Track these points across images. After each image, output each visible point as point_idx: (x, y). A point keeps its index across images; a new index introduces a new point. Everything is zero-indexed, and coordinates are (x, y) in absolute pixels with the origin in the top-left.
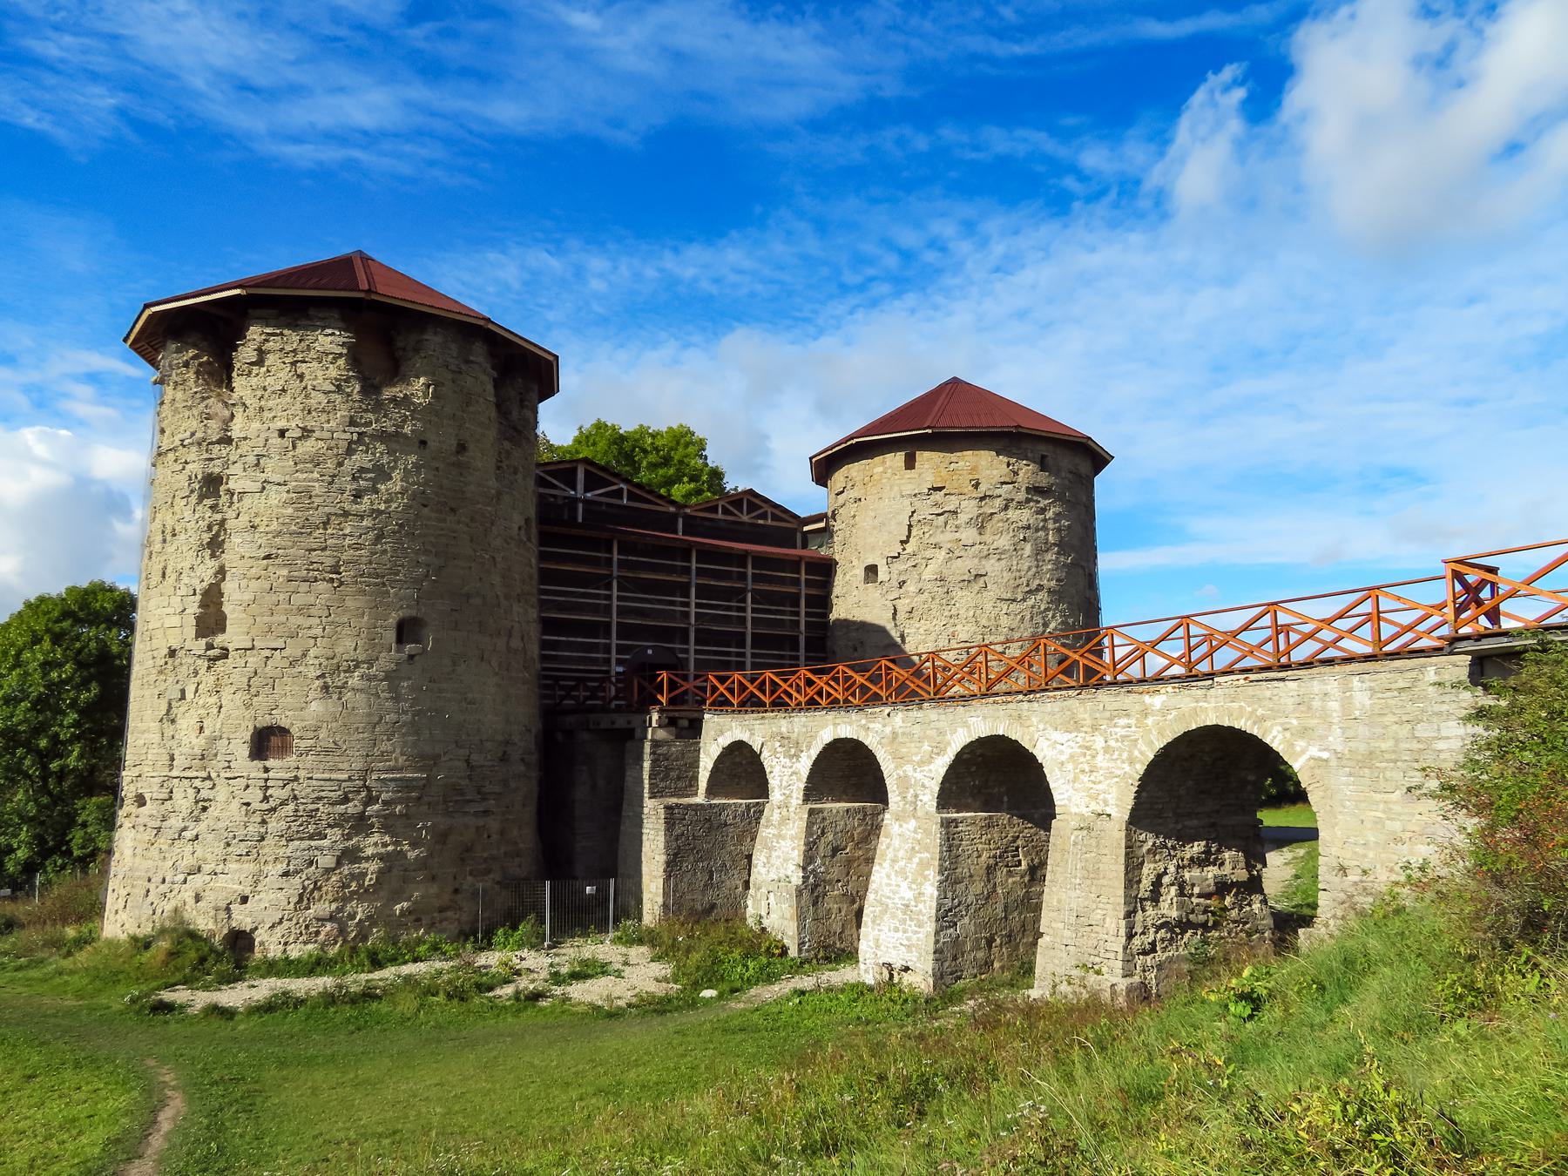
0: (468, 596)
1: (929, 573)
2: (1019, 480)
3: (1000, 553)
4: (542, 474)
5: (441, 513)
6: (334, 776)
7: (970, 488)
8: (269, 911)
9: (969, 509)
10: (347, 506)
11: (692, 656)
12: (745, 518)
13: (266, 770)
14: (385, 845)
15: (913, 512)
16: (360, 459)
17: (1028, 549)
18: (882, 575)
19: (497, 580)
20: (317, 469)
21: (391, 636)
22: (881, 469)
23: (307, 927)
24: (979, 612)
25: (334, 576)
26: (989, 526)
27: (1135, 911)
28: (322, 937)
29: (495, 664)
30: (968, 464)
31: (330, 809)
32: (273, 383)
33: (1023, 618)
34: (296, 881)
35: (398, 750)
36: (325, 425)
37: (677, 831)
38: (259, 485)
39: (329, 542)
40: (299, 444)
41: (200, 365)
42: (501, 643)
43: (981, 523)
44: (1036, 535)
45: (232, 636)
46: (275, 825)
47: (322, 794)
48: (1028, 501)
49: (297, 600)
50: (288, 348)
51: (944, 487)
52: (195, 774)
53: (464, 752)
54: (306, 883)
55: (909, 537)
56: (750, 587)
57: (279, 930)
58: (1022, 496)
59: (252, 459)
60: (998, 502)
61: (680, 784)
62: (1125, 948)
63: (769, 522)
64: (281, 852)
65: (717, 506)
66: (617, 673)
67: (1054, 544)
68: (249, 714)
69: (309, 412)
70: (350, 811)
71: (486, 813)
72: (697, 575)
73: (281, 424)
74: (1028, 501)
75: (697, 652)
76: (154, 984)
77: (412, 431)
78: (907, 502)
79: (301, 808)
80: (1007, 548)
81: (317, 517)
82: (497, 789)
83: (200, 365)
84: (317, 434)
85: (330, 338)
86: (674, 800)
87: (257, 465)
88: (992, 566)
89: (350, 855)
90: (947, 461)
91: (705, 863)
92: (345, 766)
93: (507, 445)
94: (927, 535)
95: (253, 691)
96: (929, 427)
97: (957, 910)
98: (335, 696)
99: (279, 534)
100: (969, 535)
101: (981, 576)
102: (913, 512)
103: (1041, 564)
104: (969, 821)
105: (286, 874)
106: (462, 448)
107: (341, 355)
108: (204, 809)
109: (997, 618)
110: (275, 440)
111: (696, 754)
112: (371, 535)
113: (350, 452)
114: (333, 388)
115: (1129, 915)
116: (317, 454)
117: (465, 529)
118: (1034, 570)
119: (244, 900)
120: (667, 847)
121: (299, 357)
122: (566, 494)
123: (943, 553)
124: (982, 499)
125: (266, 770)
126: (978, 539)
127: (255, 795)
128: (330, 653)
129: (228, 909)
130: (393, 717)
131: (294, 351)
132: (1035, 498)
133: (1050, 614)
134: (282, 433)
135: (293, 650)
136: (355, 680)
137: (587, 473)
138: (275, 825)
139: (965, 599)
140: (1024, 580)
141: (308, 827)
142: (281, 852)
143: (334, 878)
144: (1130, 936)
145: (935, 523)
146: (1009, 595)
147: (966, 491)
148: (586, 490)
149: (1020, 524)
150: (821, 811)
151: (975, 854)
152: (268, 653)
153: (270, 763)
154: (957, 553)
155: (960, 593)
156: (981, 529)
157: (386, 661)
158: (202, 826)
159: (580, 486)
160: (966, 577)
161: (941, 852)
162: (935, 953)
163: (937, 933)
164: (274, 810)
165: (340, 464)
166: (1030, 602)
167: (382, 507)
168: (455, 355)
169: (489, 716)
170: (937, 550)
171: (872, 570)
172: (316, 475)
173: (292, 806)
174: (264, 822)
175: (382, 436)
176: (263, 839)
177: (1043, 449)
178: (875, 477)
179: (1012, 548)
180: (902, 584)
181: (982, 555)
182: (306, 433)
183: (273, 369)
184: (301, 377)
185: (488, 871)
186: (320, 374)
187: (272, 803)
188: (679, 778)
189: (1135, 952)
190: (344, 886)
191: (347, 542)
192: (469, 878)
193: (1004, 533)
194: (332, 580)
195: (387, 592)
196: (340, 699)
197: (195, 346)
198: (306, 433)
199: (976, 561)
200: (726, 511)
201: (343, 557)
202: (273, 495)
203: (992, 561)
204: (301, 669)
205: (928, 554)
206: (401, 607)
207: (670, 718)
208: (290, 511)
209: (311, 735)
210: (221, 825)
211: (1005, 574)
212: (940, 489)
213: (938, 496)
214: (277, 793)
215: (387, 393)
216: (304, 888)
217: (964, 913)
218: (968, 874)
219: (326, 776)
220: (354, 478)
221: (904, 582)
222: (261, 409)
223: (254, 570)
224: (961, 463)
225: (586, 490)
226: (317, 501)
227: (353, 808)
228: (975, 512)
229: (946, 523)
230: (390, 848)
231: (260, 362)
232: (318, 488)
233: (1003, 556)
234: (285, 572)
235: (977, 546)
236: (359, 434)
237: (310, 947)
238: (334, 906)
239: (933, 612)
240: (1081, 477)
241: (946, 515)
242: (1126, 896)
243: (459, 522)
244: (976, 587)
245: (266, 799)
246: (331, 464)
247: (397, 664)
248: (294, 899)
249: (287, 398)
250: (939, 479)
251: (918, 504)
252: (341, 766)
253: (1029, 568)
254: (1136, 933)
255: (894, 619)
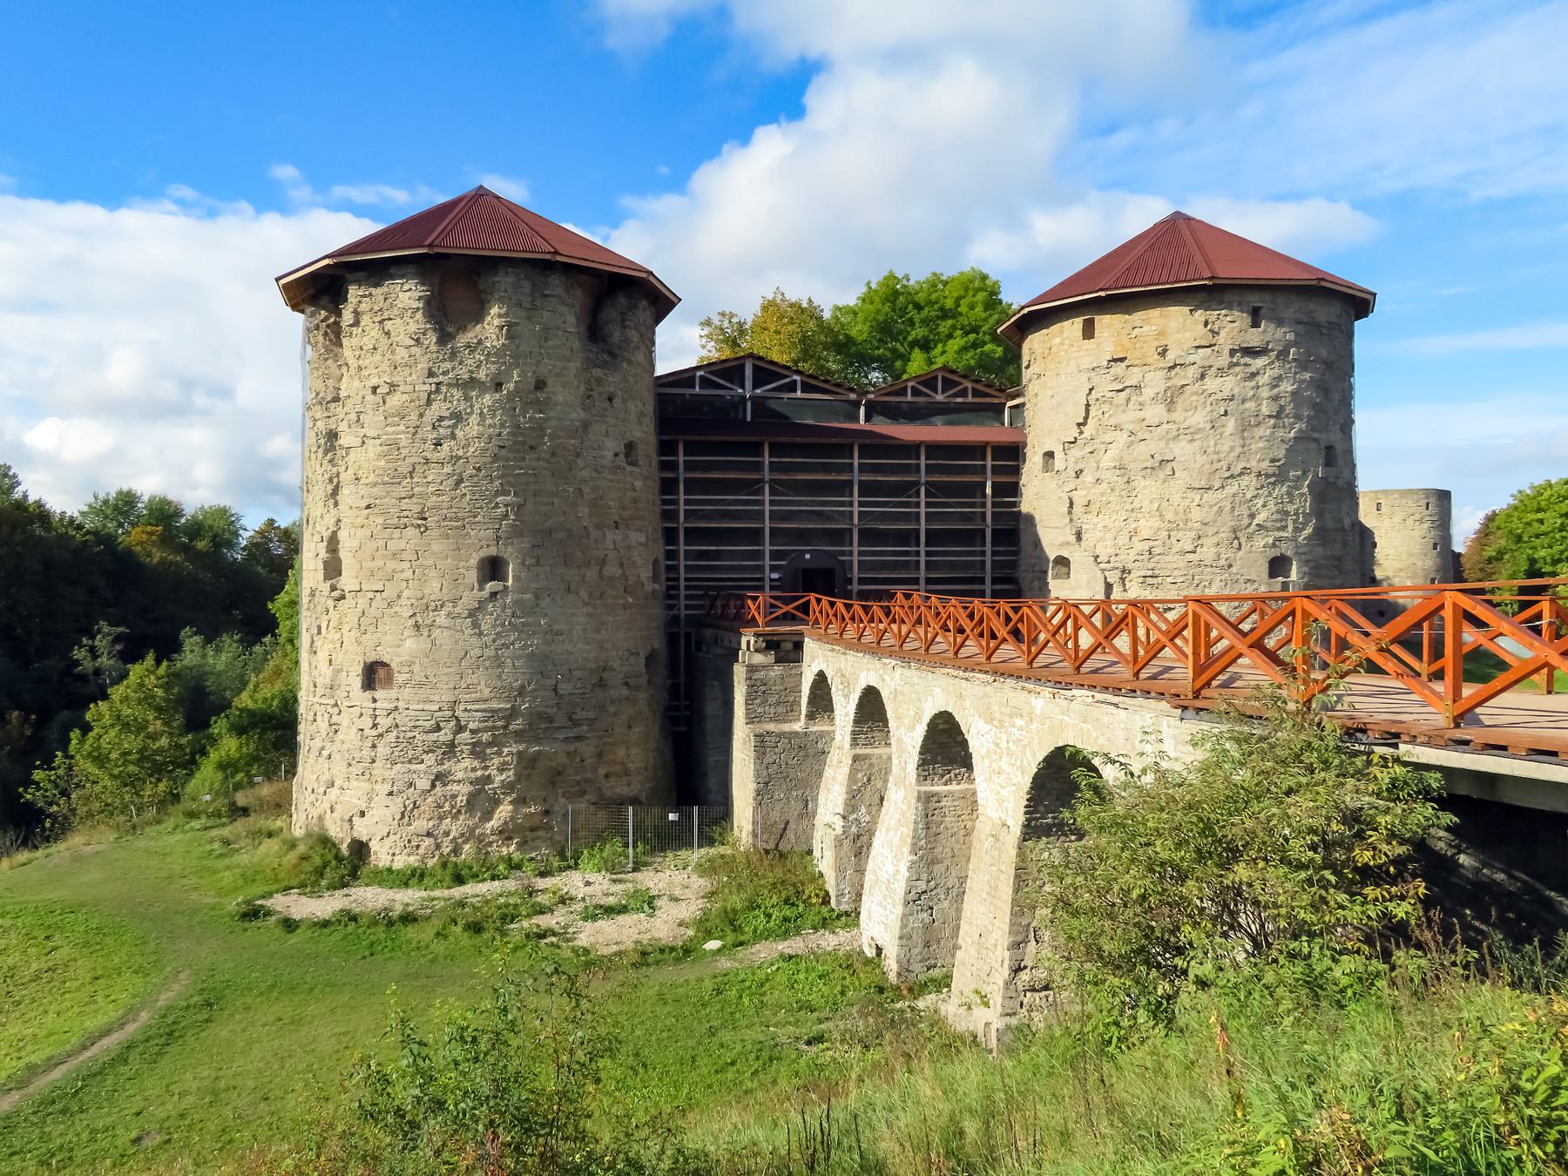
0: (550, 532)
1: (1107, 461)
2: (1222, 341)
3: (1192, 434)
4: (708, 376)
5: (519, 451)
6: (426, 708)
7: (1156, 357)
8: (379, 826)
9: (1155, 382)
10: (428, 455)
11: (856, 558)
12: (940, 397)
13: (375, 701)
14: (474, 770)
15: (1091, 390)
16: (439, 408)
17: (1231, 424)
18: (1059, 463)
19: (584, 511)
20: (403, 422)
21: (472, 576)
22: (1058, 340)
23: (409, 841)
24: (1165, 504)
25: (420, 522)
26: (1180, 400)
27: (1026, 941)
28: (421, 851)
29: (584, 594)
30: (1154, 328)
31: (425, 737)
32: (368, 342)
33: (1221, 510)
34: (399, 800)
35: (483, 683)
36: (409, 379)
37: (769, 759)
38: (359, 441)
39: (416, 490)
40: (388, 399)
41: (328, 326)
42: (592, 574)
43: (1170, 399)
44: (1242, 407)
45: (347, 581)
46: (383, 750)
47: (418, 723)
48: (1232, 365)
49: (393, 546)
50: (376, 308)
51: (1125, 358)
52: (327, 701)
53: (550, 682)
54: (407, 802)
55: (1086, 418)
56: (923, 480)
57: (388, 842)
58: (1224, 360)
59: (353, 416)
60: (1192, 372)
61: (780, 710)
62: (1007, 984)
63: (970, 399)
64: (387, 774)
65: (906, 387)
66: (771, 580)
67: (1270, 416)
68: (360, 650)
69: (396, 368)
70: (441, 739)
71: (578, 738)
72: (860, 471)
73: (374, 381)
74: (1232, 365)
75: (687, 608)
76: (274, 887)
77: (487, 375)
78: (1084, 377)
79: (402, 735)
80: (1201, 426)
81: (404, 468)
82: (591, 715)
83: (328, 326)
84: (401, 388)
85: (408, 294)
86: (771, 727)
87: (358, 421)
88: (1182, 450)
89: (440, 778)
90: (1129, 327)
91: (800, 792)
92: (436, 698)
93: (597, 372)
94: (1107, 415)
95: (363, 628)
96: (1101, 290)
97: (933, 893)
98: (426, 633)
99: (375, 485)
100: (1155, 413)
101: (1168, 461)
102: (1091, 390)
103: (1248, 442)
104: (957, 795)
105: (391, 794)
106: (540, 385)
107: (418, 309)
108: (336, 731)
109: (1187, 510)
110: (370, 398)
111: (797, 678)
112: (451, 482)
113: (429, 402)
114: (413, 343)
115: (1016, 946)
116: (404, 407)
117: (546, 465)
118: (1238, 450)
119: (363, 814)
120: (758, 775)
121: (386, 315)
122: (732, 393)
123: (1125, 436)
124: (1171, 368)
125: (375, 701)
126: (1165, 416)
127: (366, 722)
128: (420, 595)
129: (350, 820)
130: (478, 652)
131: (381, 310)
132: (1243, 361)
133: (1260, 502)
134: (374, 389)
135: (390, 593)
136: (441, 619)
137: (755, 367)
138: (383, 750)
139: (1148, 489)
140: (1224, 464)
141: (406, 752)
142: (387, 774)
143: (430, 799)
144: (1018, 970)
145: (1115, 401)
146: (1203, 483)
147: (1151, 360)
148: (755, 387)
149: (1220, 396)
150: (866, 757)
151: (963, 832)
152: (371, 595)
153: (379, 694)
154: (1140, 436)
155: (1142, 483)
156: (1171, 404)
157: (469, 599)
158: (335, 747)
159: (748, 383)
160: (1149, 464)
161: (916, 830)
162: (900, 938)
163: (905, 916)
164: (381, 735)
165: (421, 415)
166: (1230, 490)
167: (460, 453)
168: (528, 292)
169: (579, 645)
170: (1119, 433)
171: (1049, 455)
172: (402, 428)
173: (395, 733)
174: (374, 746)
175: (457, 384)
176: (374, 761)
177: (1255, 300)
178: (1054, 350)
179: (1209, 426)
180: (1078, 474)
181: (1170, 436)
182: (393, 387)
183: (367, 329)
184: (388, 334)
185: (584, 793)
186: (402, 329)
187: (380, 730)
188: (778, 703)
189: (1020, 988)
190: (439, 806)
191: (431, 489)
192: (562, 800)
193: (1199, 408)
194: (419, 526)
195: (468, 534)
196: (429, 636)
197: (324, 308)
198: (393, 387)
199: (1162, 444)
200: (916, 392)
201: (428, 504)
202: (370, 449)
203: (1183, 443)
204: (397, 609)
205: (1108, 437)
206: (482, 547)
207: (767, 642)
208: (383, 463)
209: (407, 669)
210: (345, 747)
211: (1198, 457)
212: (1122, 360)
213: (1119, 369)
214: (384, 722)
215: (463, 339)
216: (405, 807)
217: (943, 897)
218: (950, 855)
219: (420, 707)
220: (434, 427)
221: (1081, 471)
222: (360, 368)
223: (358, 520)
224: (1146, 328)
225: (755, 387)
226: (404, 452)
227: (445, 735)
228: (1161, 387)
229: (1128, 400)
230: (479, 773)
231: (356, 323)
232: (404, 440)
233: (1196, 437)
234: (380, 520)
235: (1164, 426)
236: (437, 384)
237: (412, 859)
238: (431, 824)
239: (1112, 505)
240: (1318, 325)
241: (1127, 391)
242: (1012, 925)
243: (539, 460)
244: (1162, 475)
245: (375, 726)
246: (414, 417)
247: (480, 602)
248: (398, 817)
249: (377, 357)
250: (1119, 349)
251: (1096, 380)
252: (432, 698)
253: (1232, 449)
254: (1025, 967)
255: (1070, 513)
